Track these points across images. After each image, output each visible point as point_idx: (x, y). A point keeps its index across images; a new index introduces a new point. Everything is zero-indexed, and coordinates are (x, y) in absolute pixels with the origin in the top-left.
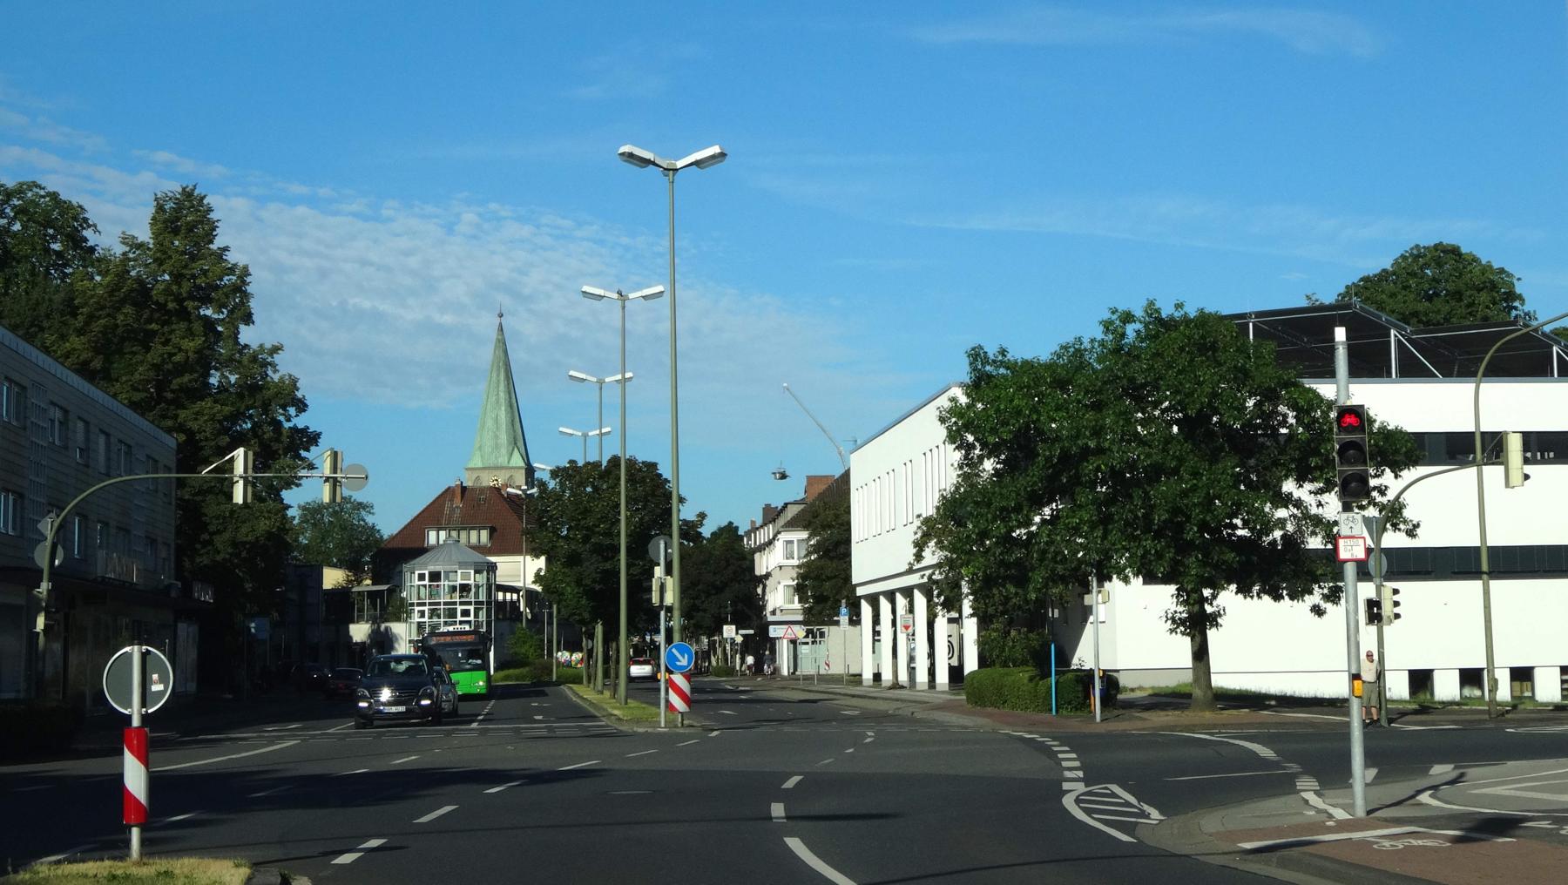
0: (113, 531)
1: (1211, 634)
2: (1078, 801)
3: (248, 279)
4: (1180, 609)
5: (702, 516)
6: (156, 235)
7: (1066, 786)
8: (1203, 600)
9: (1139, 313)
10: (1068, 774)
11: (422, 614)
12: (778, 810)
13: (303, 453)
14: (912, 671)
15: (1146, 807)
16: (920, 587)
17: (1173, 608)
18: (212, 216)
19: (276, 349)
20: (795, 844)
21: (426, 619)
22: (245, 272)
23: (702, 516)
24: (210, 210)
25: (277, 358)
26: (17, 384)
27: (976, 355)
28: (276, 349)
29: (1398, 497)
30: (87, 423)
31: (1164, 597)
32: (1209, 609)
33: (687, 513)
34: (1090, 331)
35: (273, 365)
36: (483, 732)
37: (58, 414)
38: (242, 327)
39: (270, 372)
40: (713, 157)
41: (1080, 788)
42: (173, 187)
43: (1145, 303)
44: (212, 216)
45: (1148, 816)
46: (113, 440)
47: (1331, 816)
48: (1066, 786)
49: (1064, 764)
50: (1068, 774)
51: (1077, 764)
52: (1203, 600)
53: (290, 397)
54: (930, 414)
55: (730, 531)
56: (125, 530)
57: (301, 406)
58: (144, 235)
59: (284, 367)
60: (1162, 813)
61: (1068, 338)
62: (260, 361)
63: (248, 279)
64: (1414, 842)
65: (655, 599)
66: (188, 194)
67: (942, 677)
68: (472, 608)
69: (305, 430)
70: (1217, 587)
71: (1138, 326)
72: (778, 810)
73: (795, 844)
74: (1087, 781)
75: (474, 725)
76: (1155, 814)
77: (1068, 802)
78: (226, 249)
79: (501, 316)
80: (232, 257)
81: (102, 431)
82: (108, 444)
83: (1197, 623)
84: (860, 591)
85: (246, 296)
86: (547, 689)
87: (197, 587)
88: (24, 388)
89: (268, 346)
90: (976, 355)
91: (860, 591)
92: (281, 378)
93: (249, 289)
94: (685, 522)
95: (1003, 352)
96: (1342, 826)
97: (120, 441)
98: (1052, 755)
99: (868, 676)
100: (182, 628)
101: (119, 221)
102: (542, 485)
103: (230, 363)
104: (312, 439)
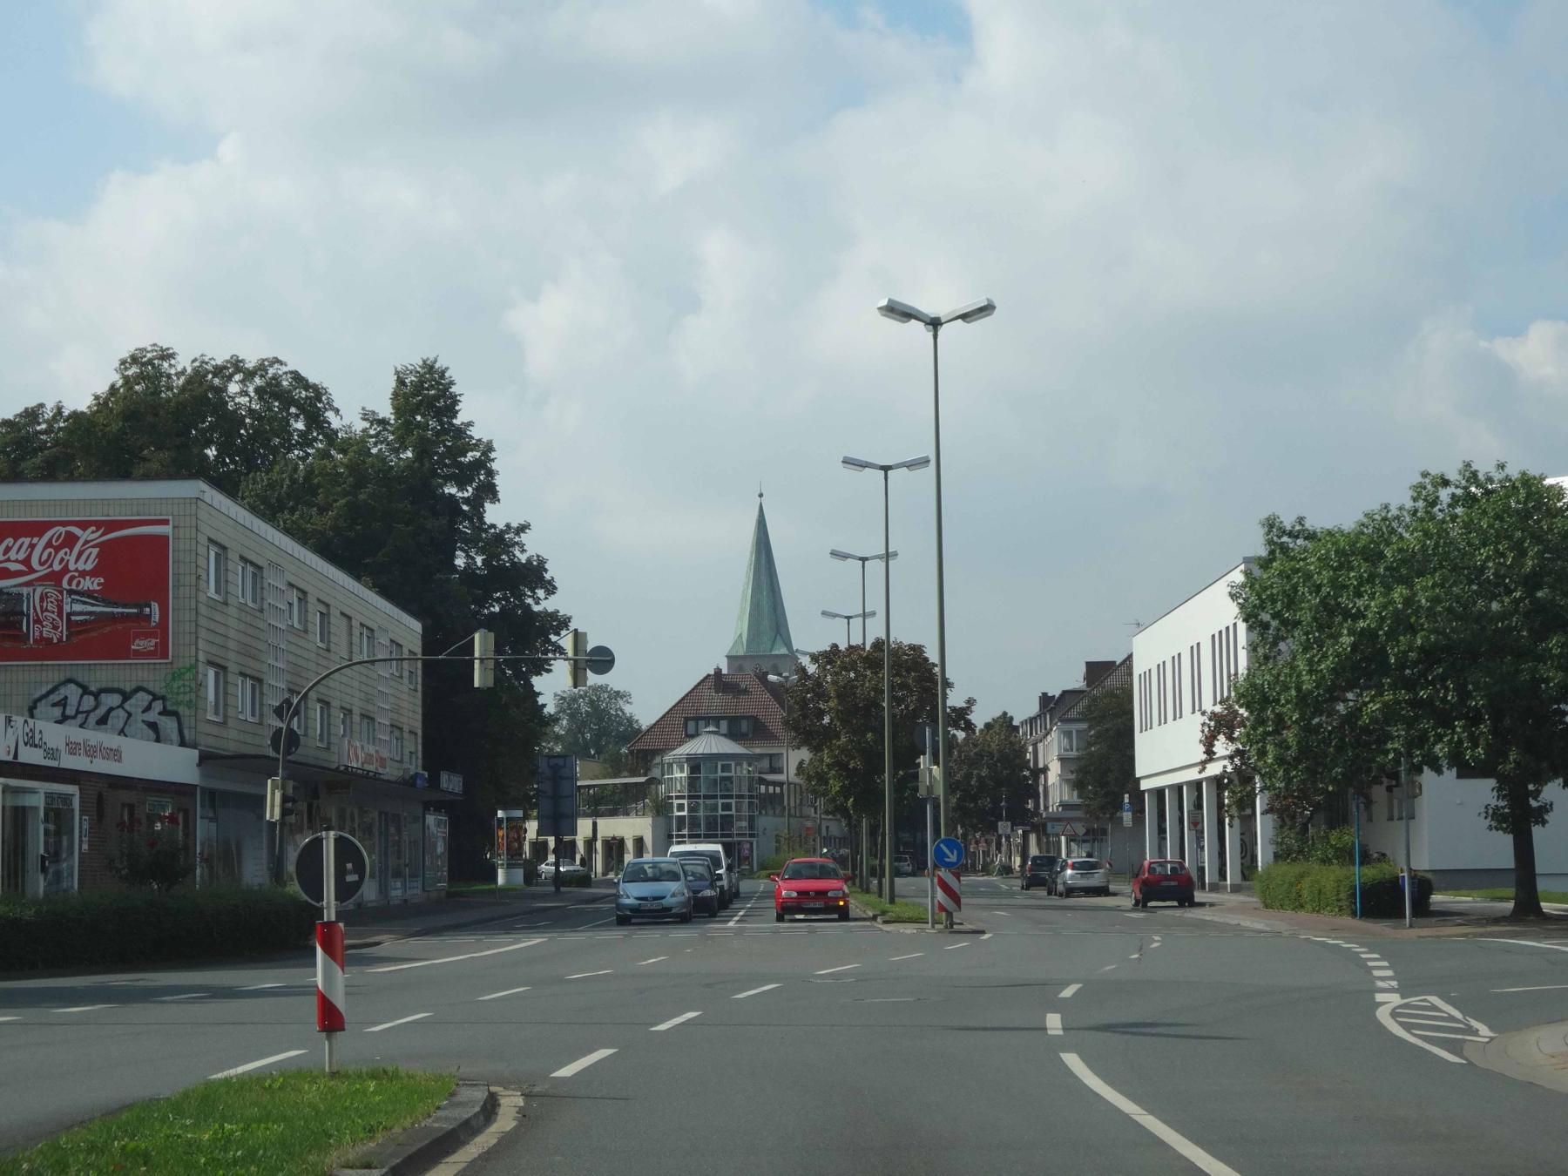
0: (356, 718)
1: (1537, 831)
3: (493, 455)
4: (1502, 803)
5: (971, 702)
6: (398, 411)
7: (1379, 997)
8: (1529, 794)
9: (1453, 476)
10: (1380, 984)
12: (1054, 1022)
13: (553, 638)
17: (1494, 802)
18: (454, 389)
19: (523, 528)
20: (1072, 1060)
22: (489, 448)
23: (971, 702)
24: (452, 383)
25: (524, 538)
26: (252, 564)
27: (1271, 524)
28: (523, 528)
29: (1410, 870)
31: (1484, 791)
32: (1534, 803)
33: (955, 699)
34: (1400, 498)
35: (522, 546)
36: (739, 932)
37: (294, 597)
38: (488, 505)
39: (517, 553)
40: (1254, 858)
41: (1395, 999)
42: (414, 359)
43: (1460, 466)
44: (454, 389)
45: (1476, 1033)
46: (354, 623)
48: (1379, 997)
49: (1376, 973)
50: (1380, 984)
51: (1389, 973)
52: (1529, 794)
53: (534, 575)
54: (1221, 589)
55: (1005, 721)
56: (368, 718)
57: (551, 588)
58: (386, 411)
59: (532, 546)
60: (1491, 1028)
61: (1374, 506)
62: (499, 542)
63: (493, 455)
66: (429, 367)
69: (554, 615)
70: (1541, 780)
71: (1450, 490)
72: (1054, 1022)
73: (1072, 1060)
74: (1403, 991)
75: (731, 924)
76: (1484, 1030)
77: (1383, 1015)
78: (470, 424)
79: (761, 495)
80: (476, 433)
83: (1519, 818)
85: (491, 473)
87: (444, 777)
88: (260, 568)
89: (515, 525)
90: (1271, 524)
91: (1145, 785)
92: (529, 560)
93: (494, 466)
94: (954, 709)
95: (1301, 520)
98: (1362, 965)
100: (431, 819)
101: (359, 398)
102: (802, 670)
103: (471, 542)
104: (564, 623)
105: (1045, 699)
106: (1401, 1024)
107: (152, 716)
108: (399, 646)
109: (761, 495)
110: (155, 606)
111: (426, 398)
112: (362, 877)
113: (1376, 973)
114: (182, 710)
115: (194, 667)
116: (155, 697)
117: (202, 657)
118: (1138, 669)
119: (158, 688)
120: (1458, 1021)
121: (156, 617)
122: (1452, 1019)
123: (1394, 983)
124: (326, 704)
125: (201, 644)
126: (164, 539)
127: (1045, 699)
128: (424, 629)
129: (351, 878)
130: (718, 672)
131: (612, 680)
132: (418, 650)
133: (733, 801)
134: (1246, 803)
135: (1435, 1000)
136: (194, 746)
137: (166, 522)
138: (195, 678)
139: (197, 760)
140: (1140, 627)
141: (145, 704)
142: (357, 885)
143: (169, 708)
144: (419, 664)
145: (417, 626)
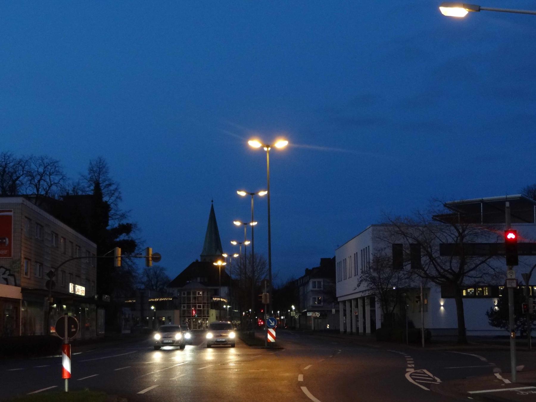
2: (411, 375)
10: (409, 366)
11: (184, 307)
14: (351, 328)
15: (436, 378)
16: (360, 298)
21: (186, 309)
30: (65, 239)
41: (412, 370)
45: (435, 381)
47: (504, 382)
50: (409, 366)
64: (533, 392)
65: (263, 301)
67: (368, 330)
68: (202, 305)
74: (415, 368)
76: (439, 380)
77: (407, 376)
81: (62, 237)
82: (65, 242)
83: (183, 335)
84: (339, 300)
86: (447, 211)
91: (339, 300)
96: (507, 386)
97: (76, 245)
99: (342, 329)
105: (307, 270)
106: (412, 378)
107: (5, 276)
108: (89, 252)
109: (212, 201)
110: (7, 239)
111: (98, 170)
112: (76, 330)
113: (408, 362)
114: (16, 274)
115: (20, 260)
116: (7, 270)
117: (22, 256)
118: (337, 261)
119: (7, 266)
120: (431, 377)
121: (7, 242)
122: (429, 377)
123: (413, 366)
124: (64, 272)
125: (22, 252)
126: (10, 217)
127: (307, 270)
128: (98, 247)
129: (74, 330)
130: (197, 261)
131: (161, 264)
132: (95, 253)
133: (202, 305)
134: (372, 305)
135: (425, 371)
136: (19, 286)
137: (11, 211)
138: (20, 263)
139: (20, 291)
140: (339, 247)
141: (3, 272)
142: (75, 333)
143: (11, 273)
144: (96, 259)
145: (95, 246)
